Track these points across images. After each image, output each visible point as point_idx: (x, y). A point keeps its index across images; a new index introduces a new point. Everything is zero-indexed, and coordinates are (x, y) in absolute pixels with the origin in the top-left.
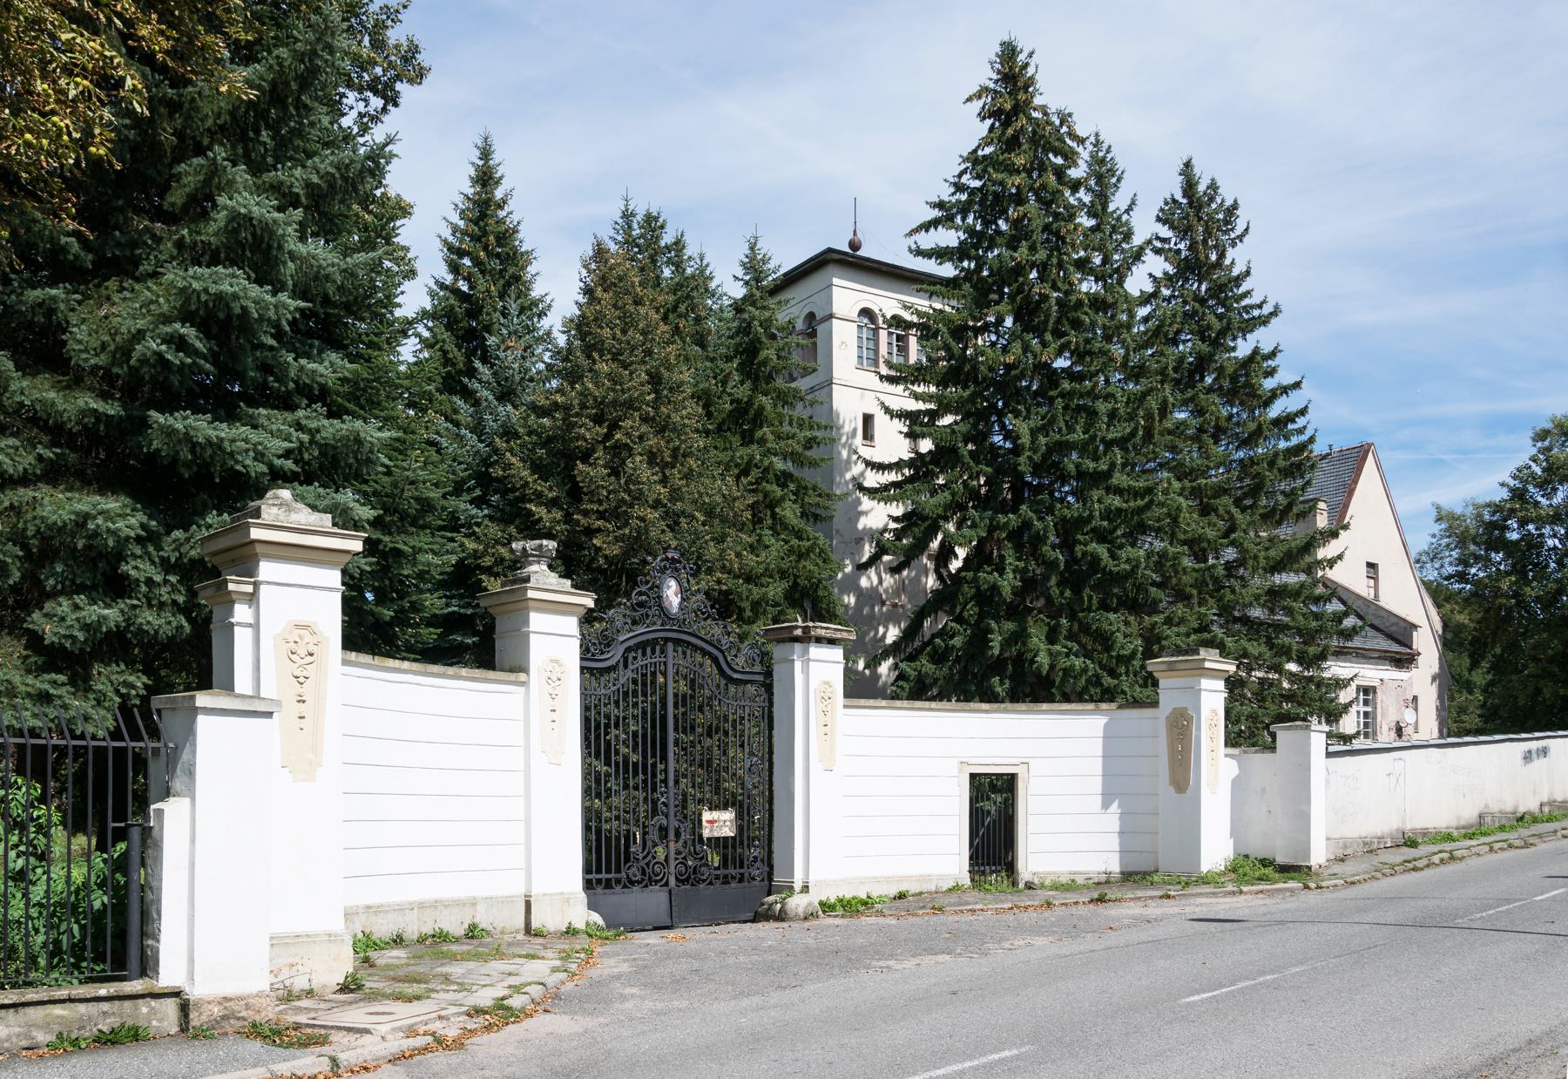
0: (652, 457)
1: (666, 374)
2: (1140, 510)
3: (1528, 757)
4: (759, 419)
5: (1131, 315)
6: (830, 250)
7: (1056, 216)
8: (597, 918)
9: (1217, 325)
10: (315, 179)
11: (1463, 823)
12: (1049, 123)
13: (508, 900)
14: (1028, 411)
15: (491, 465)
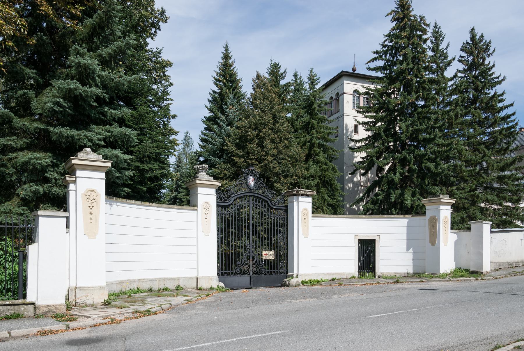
0: (272, 141)
1: (277, 114)
4: (313, 127)
5: (446, 85)
6: (343, 72)
7: (418, 52)
8: (222, 285)
10: (110, 52)
12: (416, 20)
13: (191, 278)
14: (406, 119)
15: (224, 146)
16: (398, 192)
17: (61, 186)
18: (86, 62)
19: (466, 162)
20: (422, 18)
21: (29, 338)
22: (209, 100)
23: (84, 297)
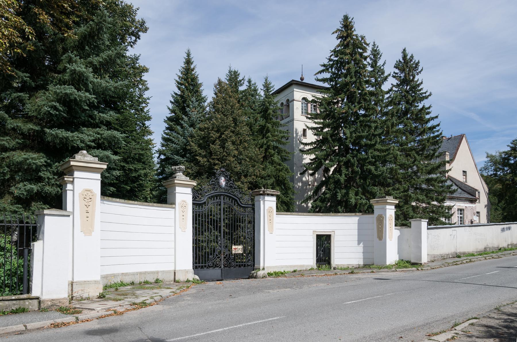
0: (233, 143)
2: (385, 156)
3: (503, 230)
4: (268, 131)
5: (383, 97)
6: (293, 80)
7: (360, 67)
8: (197, 277)
9: (411, 99)
10: (101, 60)
11: (478, 250)
12: (358, 40)
13: (169, 272)
15: (187, 146)
16: (344, 191)
17: (53, 185)
18: (81, 70)
19: (399, 165)
20: (363, 38)
21: (45, 330)
22: (171, 102)
23: (80, 291)
